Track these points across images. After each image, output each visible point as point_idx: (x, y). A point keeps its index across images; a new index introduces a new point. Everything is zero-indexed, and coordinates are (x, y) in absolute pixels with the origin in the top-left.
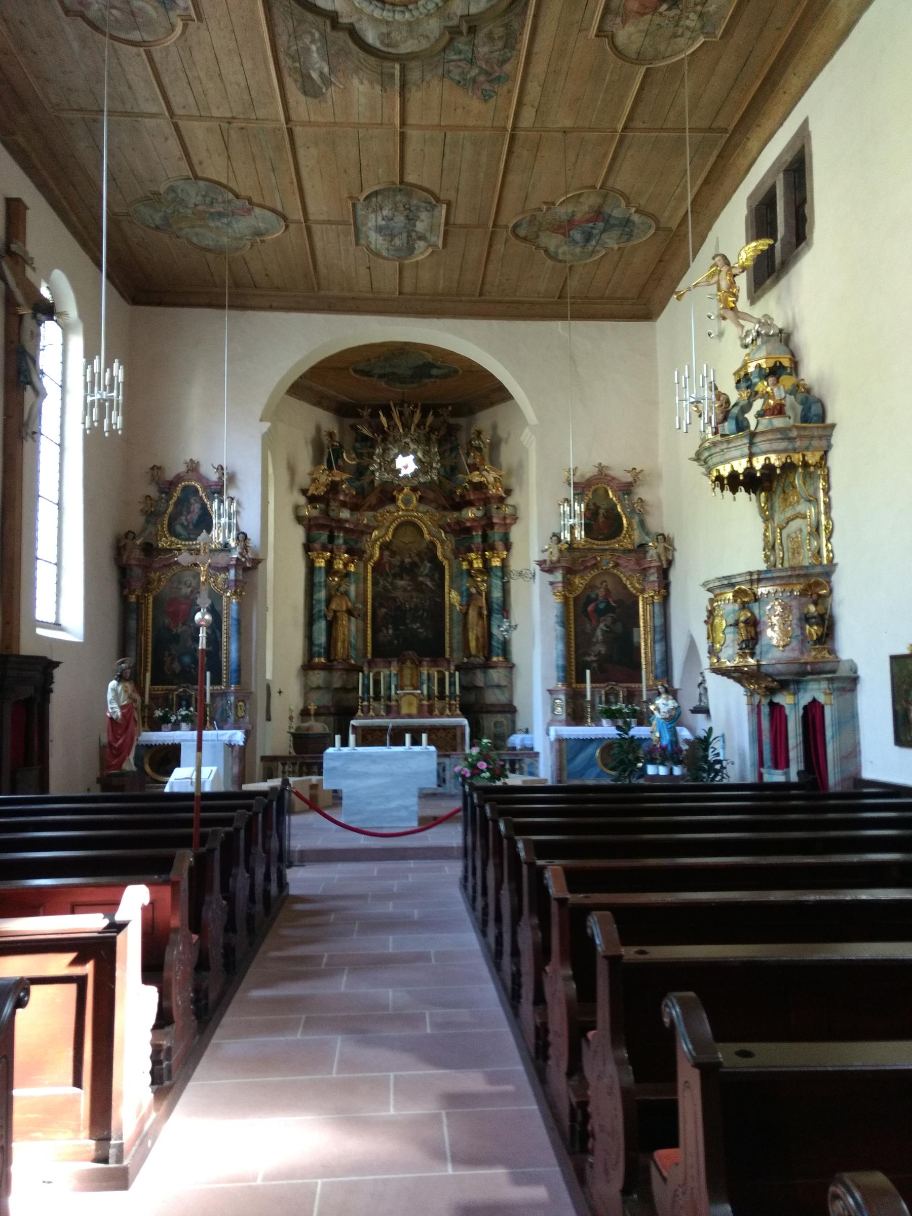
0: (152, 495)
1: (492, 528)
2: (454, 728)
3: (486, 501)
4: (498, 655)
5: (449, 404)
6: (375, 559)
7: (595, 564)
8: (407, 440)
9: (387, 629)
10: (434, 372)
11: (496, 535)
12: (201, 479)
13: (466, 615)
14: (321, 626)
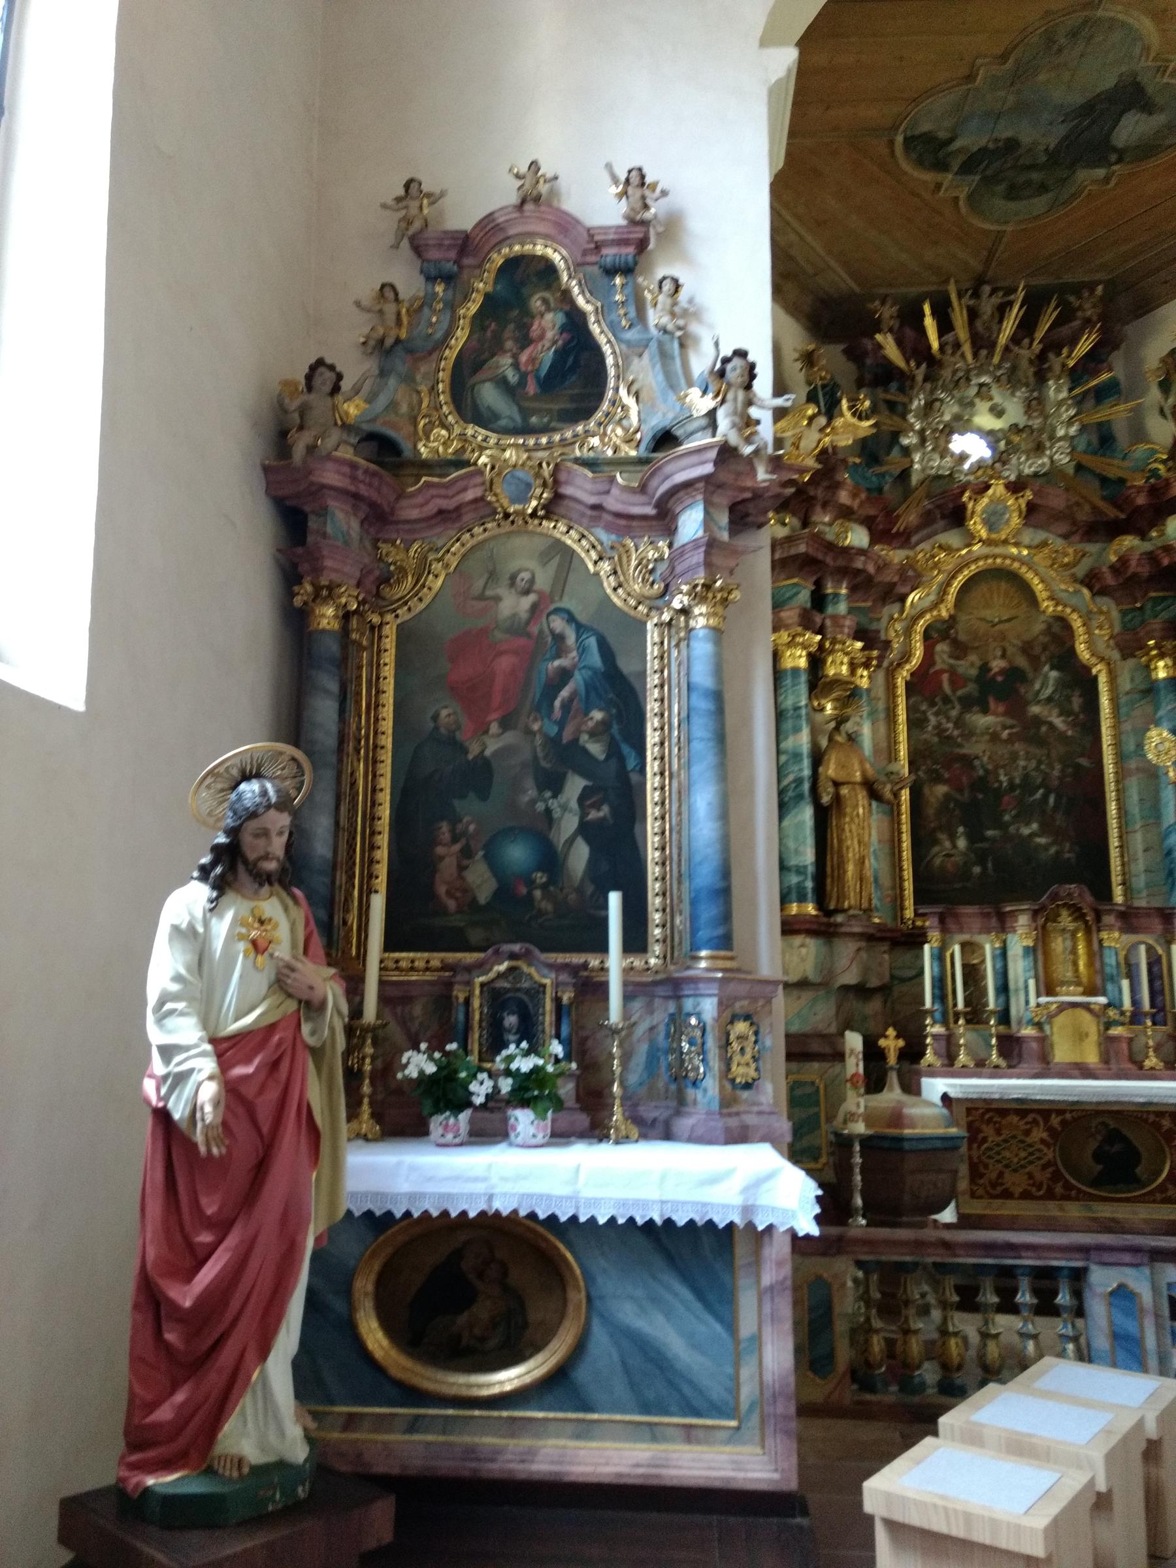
0: (400, 288)
5: (1098, 283)
8: (985, 379)
9: (953, 837)
12: (565, 226)
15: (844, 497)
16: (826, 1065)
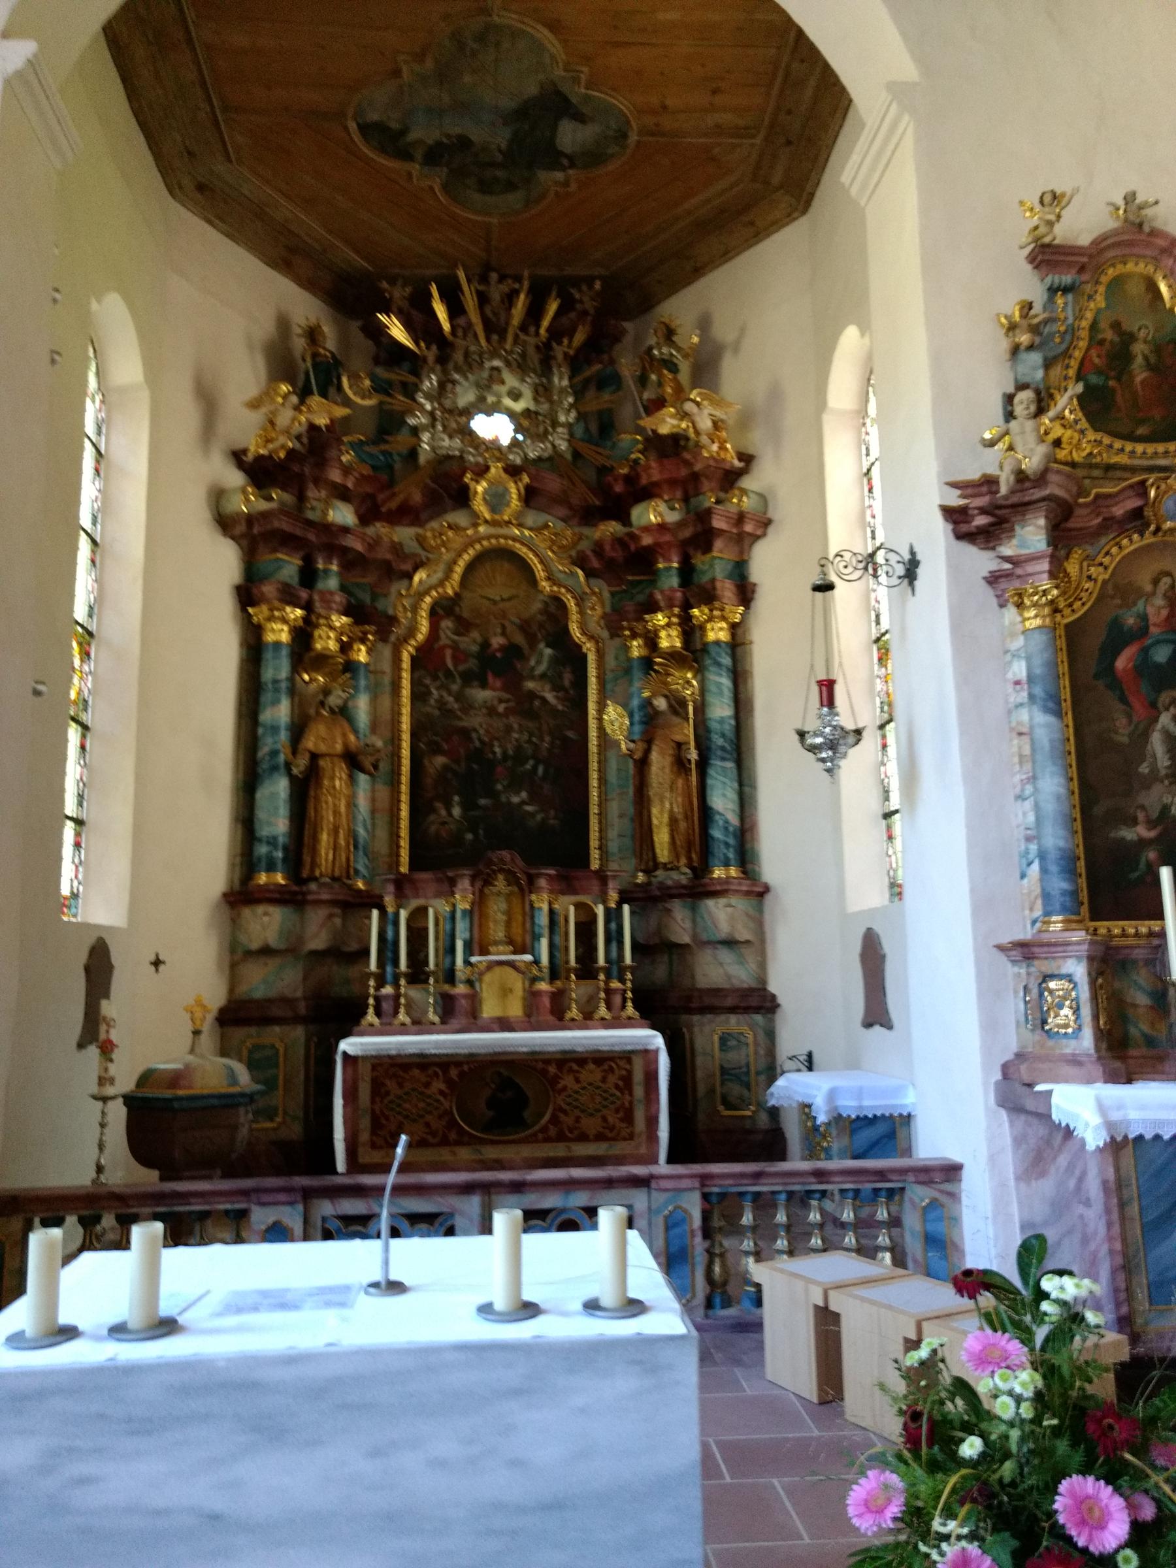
1: (707, 548)
2: (627, 1056)
4: (727, 864)
6: (420, 637)
7: (1137, 514)
8: (497, 363)
9: (448, 806)
10: (570, 136)
11: (716, 565)
13: (642, 764)
14: (277, 791)
15: (335, 475)
16: (287, 1028)
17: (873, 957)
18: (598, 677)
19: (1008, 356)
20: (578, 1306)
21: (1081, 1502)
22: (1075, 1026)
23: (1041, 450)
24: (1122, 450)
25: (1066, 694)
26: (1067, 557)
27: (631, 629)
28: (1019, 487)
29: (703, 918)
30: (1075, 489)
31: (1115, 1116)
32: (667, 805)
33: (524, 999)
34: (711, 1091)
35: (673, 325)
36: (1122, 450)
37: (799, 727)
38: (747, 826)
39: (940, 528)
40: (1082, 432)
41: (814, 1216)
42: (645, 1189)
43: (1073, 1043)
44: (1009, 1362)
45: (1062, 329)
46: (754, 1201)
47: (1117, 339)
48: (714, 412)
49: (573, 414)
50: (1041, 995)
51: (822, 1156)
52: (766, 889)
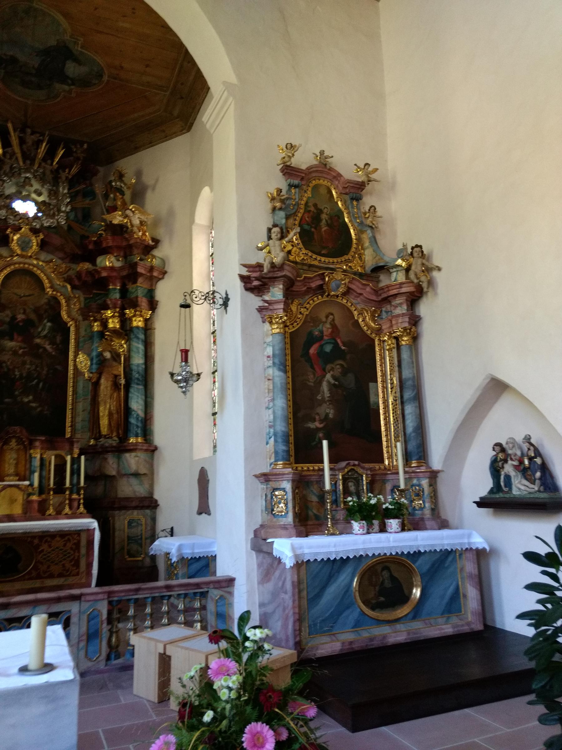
1: (135, 282)
2: (77, 533)
3: (127, 250)
4: (137, 436)
7: (321, 287)
10: (71, 69)
11: (139, 289)
13: (96, 385)
17: (203, 481)
18: (75, 339)
19: (271, 211)
20: (16, 670)
21: (255, 735)
22: (286, 512)
23: (282, 255)
24: (316, 259)
25: (289, 363)
26: (292, 303)
27: (94, 317)
28: (272, 270)
29: (123, 462)
30: (295, 274)
31: (299, 552)
32: (108, 406)
33: (23, 505)
34: (122, 548)
35: (123, 172)
36: (316, 259)
37: (171, 371)
38: (148, 418)
39: (238, 285)
40: (300, 249)
41: (165, 608)
42: (79, 601)
43: (284, 519)
44: (229, 672)
45: (294, 203)
46: (135, 603)
47: (315, 211)
48: (141, 217)
49: (69, 208)
50: (272, 498)
51: (174, 578)
52: (156, 448)
